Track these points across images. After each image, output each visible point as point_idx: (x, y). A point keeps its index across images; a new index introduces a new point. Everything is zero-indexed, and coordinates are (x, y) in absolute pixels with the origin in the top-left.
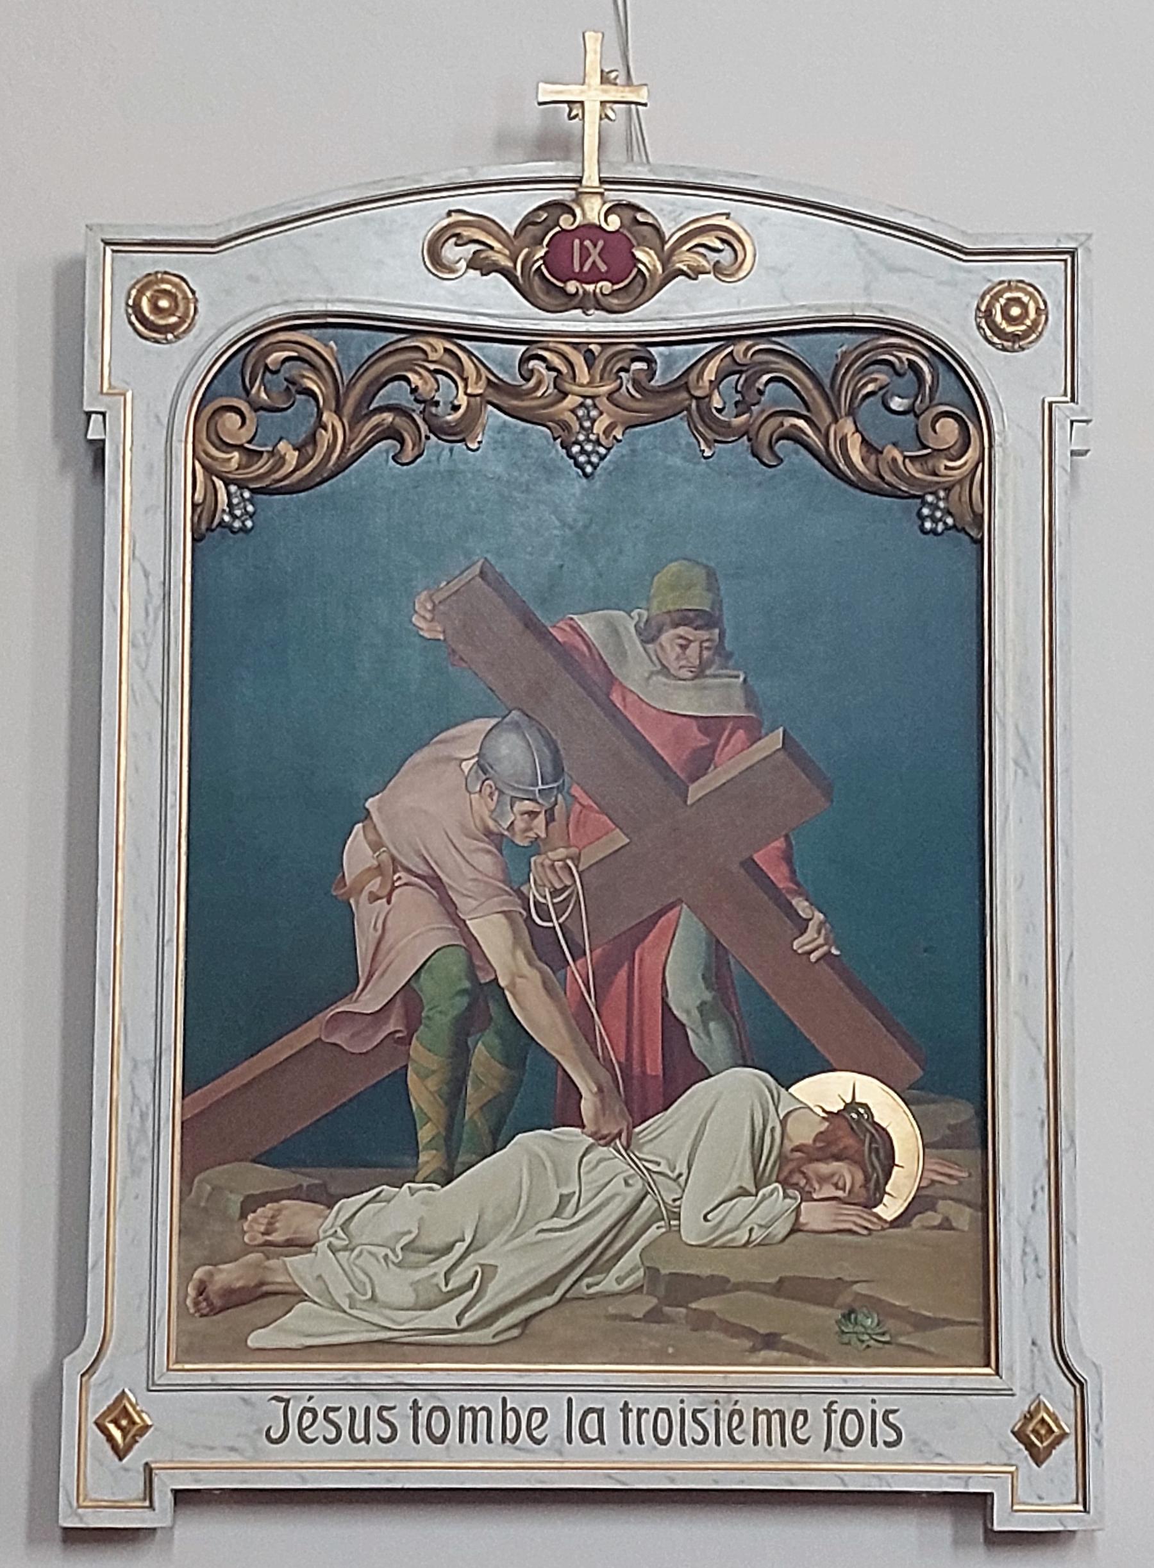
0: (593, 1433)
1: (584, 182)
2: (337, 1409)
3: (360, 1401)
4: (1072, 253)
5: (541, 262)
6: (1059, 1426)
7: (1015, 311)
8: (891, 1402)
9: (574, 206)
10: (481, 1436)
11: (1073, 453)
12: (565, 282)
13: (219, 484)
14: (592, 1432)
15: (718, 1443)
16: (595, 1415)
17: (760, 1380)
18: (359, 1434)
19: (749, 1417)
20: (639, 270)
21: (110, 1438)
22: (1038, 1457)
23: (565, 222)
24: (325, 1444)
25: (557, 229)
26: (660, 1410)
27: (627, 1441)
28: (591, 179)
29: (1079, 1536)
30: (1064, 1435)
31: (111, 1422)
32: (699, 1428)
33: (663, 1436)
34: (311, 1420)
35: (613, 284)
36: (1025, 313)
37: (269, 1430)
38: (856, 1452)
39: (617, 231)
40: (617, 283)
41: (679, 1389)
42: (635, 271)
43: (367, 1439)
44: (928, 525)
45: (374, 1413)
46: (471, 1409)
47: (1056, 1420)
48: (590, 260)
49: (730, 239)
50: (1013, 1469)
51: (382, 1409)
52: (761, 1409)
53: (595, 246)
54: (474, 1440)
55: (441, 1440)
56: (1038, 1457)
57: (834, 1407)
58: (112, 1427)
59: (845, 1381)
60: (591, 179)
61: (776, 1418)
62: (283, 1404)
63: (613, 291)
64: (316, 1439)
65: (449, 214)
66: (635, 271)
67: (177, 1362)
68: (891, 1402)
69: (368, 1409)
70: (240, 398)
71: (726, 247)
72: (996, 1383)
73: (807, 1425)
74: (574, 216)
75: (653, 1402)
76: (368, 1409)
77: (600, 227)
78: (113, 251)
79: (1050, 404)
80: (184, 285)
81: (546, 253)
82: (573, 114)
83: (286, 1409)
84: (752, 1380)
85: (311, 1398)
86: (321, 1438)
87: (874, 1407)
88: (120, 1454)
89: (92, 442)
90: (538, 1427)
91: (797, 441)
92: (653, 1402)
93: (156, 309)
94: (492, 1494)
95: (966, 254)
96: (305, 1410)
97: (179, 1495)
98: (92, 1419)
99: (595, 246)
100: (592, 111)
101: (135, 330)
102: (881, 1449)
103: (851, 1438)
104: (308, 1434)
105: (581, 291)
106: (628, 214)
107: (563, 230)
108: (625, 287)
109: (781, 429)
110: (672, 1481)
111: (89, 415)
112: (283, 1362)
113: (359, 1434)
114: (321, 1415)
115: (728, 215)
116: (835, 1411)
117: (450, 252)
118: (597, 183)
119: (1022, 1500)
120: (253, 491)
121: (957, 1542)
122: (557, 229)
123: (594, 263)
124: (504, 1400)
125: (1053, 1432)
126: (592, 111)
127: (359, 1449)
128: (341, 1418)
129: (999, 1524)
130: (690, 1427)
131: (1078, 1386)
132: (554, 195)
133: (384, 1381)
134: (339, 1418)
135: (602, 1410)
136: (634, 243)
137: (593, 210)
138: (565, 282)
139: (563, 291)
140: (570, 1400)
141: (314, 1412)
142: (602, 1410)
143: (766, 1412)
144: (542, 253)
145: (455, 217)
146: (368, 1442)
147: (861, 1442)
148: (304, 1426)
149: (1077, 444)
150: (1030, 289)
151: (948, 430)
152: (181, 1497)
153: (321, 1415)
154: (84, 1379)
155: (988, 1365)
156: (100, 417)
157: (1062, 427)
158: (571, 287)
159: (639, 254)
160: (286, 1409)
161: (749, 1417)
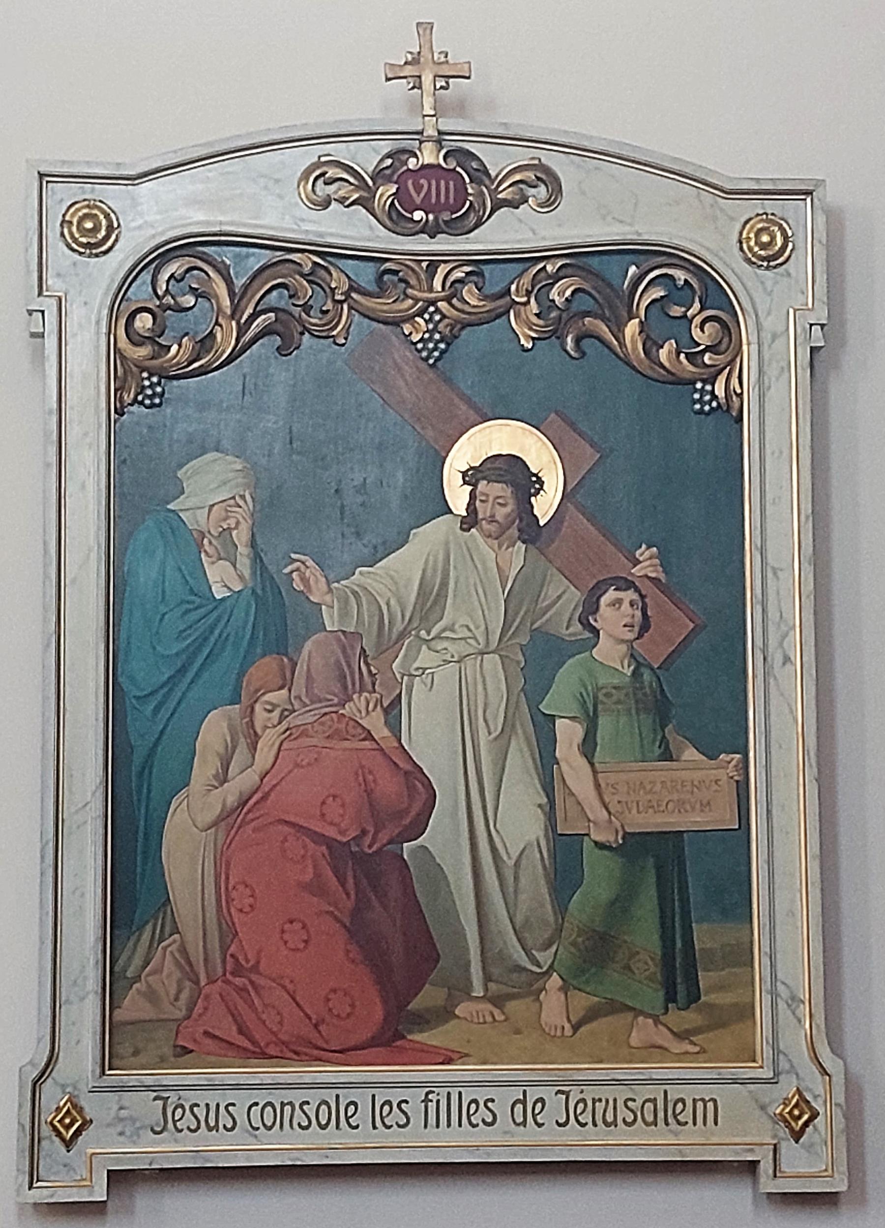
3: (212, 1098)
4: (41, 175)
7: (89, 225)
9: (418, 153)
10: (700, 1120)
12: (411, 213)
15: (338, 1127)
18: (212, 1123)
19: (689, 1103)
21: (59, 1134)
22: (797, 1136)
23: (412, 163)
25: (405, 168)
27: (374, 1127)
30: (814, 1115)
33: (520, 1120)
35: (452, 213)
38: (235, 1134)
39: (454, 169)
40: (456, 213)
42: (468, 203)
43: (615, 1123)
44: (157, 401)
45: (620, 1103)
48: (422, 195)
52: (707, 1099)
54: (705, 1124)
55: (323, 1127)
57: (430, 1097)
61: (710, 1105)
66: (468, 203)
67: (110, 1069)
69: (218, 1105)
71: (543, 186)
73: (391, 1116)
74: (416, 156)
76: (218, 1105)
77: (439, 166)
78: (48, 182)
79: (795, 311)
84: (177, 1080)
87: (439, 1097)
88: (68, 1144)
89: (33, 335)
90: (474, 1114)
93: (764, 246)
94: (236, 1171)
95: (135, 179)
102: (222, 1133)
103: (269, 1124)
105: (424, 220)
107: (409, 170)
108: (403, 215)
110: (248, 1160)
111: (30, 312)
113: (212, 1123)
114: (297, 1107)
116: (431, 1101)
118: (436, 134)
120: (160, 377)
124: (666, 1092)
127: (213, 1136)
128: (200, 1112)
129: (102, 1197)
137: (429, 155)
139: (412, 219)
140: (460, 1093)
141: (182, 1107)
143: (703, 1100)
153: (297, 1107)
155: (754, 1061)
156: (40, 314)
158: (418, 215)
161: (689, 1103)
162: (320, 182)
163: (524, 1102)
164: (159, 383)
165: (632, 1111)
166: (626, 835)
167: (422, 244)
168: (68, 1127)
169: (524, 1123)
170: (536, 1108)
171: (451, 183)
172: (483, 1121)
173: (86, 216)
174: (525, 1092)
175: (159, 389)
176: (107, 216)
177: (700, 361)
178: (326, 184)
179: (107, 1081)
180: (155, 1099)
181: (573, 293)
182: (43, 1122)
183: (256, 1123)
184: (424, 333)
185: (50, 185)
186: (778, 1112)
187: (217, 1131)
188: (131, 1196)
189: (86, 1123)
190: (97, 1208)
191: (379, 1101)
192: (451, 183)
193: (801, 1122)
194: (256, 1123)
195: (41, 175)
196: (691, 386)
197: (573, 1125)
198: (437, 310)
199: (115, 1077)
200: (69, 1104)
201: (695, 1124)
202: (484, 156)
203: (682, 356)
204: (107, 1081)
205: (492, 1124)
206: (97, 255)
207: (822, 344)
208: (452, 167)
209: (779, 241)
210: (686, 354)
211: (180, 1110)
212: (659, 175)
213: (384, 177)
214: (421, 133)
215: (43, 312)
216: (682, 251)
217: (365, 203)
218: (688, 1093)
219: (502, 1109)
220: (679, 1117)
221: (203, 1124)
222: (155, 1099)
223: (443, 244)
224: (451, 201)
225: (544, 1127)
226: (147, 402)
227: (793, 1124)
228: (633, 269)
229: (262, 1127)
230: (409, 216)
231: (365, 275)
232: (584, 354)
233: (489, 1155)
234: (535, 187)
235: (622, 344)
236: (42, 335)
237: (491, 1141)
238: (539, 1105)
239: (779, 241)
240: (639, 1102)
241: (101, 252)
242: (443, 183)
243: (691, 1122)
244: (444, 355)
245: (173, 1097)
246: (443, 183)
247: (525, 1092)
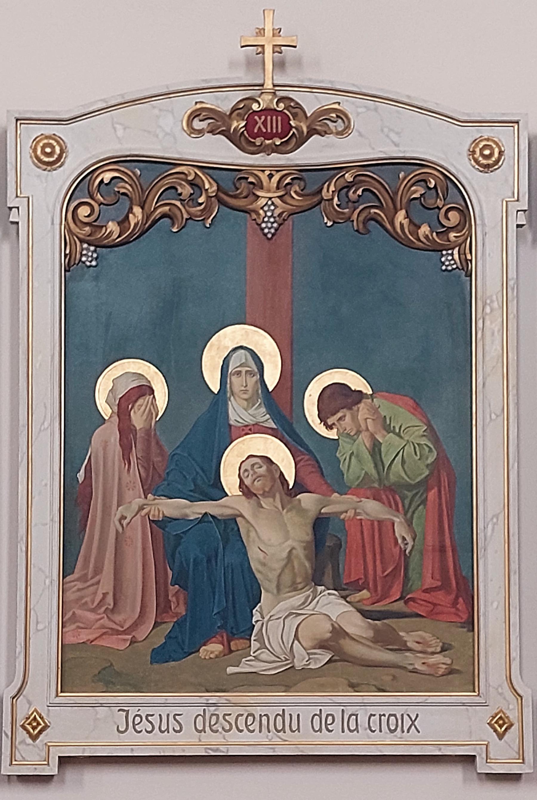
0: (200, 727)
1: (265, 87)
3: (164, 711)
5: (244, 129)
6: (44, 722)
8: (178, 710)
10: (264, 729)
11: (518, 226)
13: (78, 243)
14: (353, 727)
16: (354, 717)
17: (108, 700)
20: (294, 133)
21: (28, 732)
22: (501, 736)
23: (255, 107)
24: (145, 733)
25: (251, 111)
26: (390, 715)
28: (269, 85)
29: (523, 776)
30: (511, 725)
31: (28, 724)
32: (150, 725)
34: (252, 720)
35: (281, 139)
36: (491, 155)
37: (118, 727)
41: (340, 704)
43: (168, 730)
45: (171, 718)
47: (42, 718)
49: (342, 115)
50: (486, 743)
52: (263, 715)
53: (260, 119)
56: (501, 736)
58: (496, 725)
59: (331, 700)
60: (269, 85)
62: (125, 713)
63: (282, 143)
64: (142, 731)
65: (196, 103)
67: (61, 692)
68: (178, 710)
70: (87, 198)
71: (340, 120)
72: (477, 700)
74: (259, 104)
75: (388, 710)
77: (275, 110)
79: (507, 202)
80: (347, 135)
81: (246, 124)
82: (258, 52)
83: (127, 717)
85: (139, 710)
86: (144, 731)
88: (34, 738)
89: (12, 223)
91: (377, 221)
92: (388, 710)
94: (406, 757)
96: (137, 715)
97: (61, 758)
98: (20, 723)
99: (260, 119)
100: (268, 50)
101: (33, 162)
103: (179, 729)
104: (329, 727)
106: (287, 102)
109: (370, 215)
111: (10, 209)
112: (333, 692)
114: (144, 718)
115: (339, 103)
117: (197, 124)
118: (271, 86)
119: (492, 757)
121: (465, 780)
122: (286, 111)
123: (259, 128)
125: (41, 725)
126: (268, 50)
128: (155, 720)
130: (172, 722)
131: (519, 699)
132: (247, 93)
133: (94, 702)
134: (180, 718)
135: (358, 714)
136: (291, 117)
138: (255, 139)
141: (217, 716)
142: (358, 714)
144: (243, 124)
145: (198, 106)
146: (321, 732)
147: (128, 731)
148: (249, 724)
149: (520, 221)
150: (59, 139)
151: (454, 217)
152: (64, 761)
153: (144, 718)
154: (14, 700)
155: (474, 691)
156: (16, 209)
157: (512, 214)
158: (258, 141)
159: (292, 123)
160: (127, 717)
162: (196, 119)
163: (283, 716)
164: (95, 251)
165: (177, 721)
166: (164, 516)
167: (259, 159)
168: (501, 726)
169: (320, 730)
170: (328, 720)
171: (279, 118)
172: (223, 728)
173: (485, 147)
174: (321, 710)
176: (58, 142)
177: (446, 238)
178: (200, 121)
179: (58, 700)
180: (119, 710)
181: (363, 191)
182: (18, 725)
183: (242, 727)
184: (264, 218)
185: (22, 125)
186: (22, 723)
187: (168, 732)
188: (64, 774)
189: (46, 727)
190: (46, 779)
191: (132, 714)
192: (279, 118)
193: (503, 729)
194: (242, 727)
195: (17, 120)
196: (440, 253)
197: (144, 733)
198: (273, 204)
199: (67, 697)
200: (35, 713)
201: (381, 731)
202: (302, 102)
203: (434, 234)
204: (58, 700)
205: (179, 731)
206: (55, 170)
207: (524, 223)
208: (280, 109)
209: (58, 150)
210: (437, 233)
211: (214, 718)
212: (417, 112)
213: (238, 115)
214: (262, 85)
215: (18, 208)
216: (438, 166)
217: (225, 133)
218: (398, 711)
219: (363, 719)
220: (249, 727)
221: (234, 726)
222: (119, 710)
223: (276, 159)
224: (280, 130)
225: (333, 732)
226: (88, 264)
227: (499, 729)
228: (402, 175)
229: (245, 730)
230: (253, 140)
231: (227, 179)
232: (369, 232)
233: (132, 750)
234: (335, 122)
235: (392, 223)
236: (17, 223)
237: (235, 742)
238: (330, 718)
239: (496, 155)
240: (234, 717)
241: (57, 167)
242: (274, 118)
243: (378, 730)
244: (278, 232)
245: (133, 711)
246: (274, 118)
247: (321, 710)
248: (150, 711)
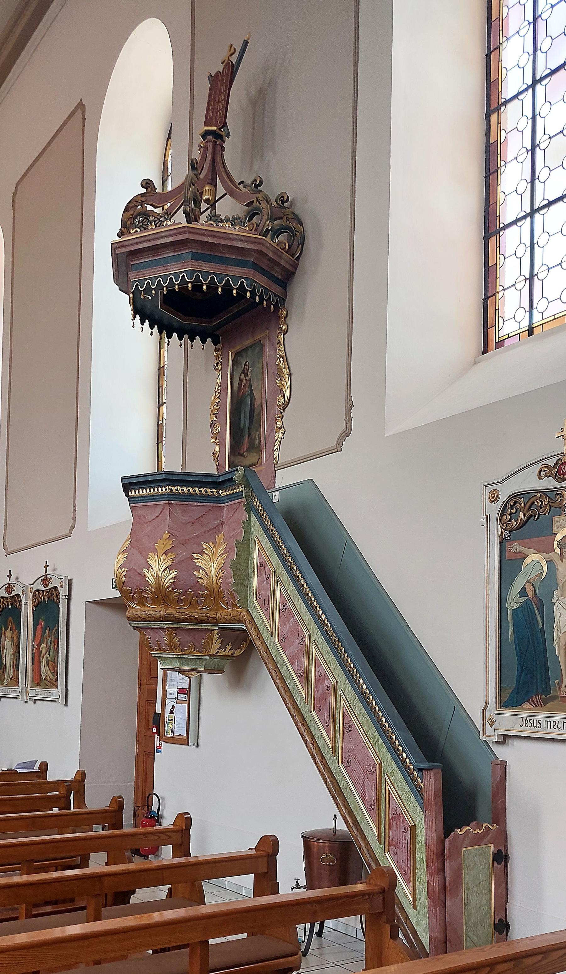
2: (531, 720)
46: (547, 721)
51: (530, 720)
175: (509, 535)
248: (531, 718)
